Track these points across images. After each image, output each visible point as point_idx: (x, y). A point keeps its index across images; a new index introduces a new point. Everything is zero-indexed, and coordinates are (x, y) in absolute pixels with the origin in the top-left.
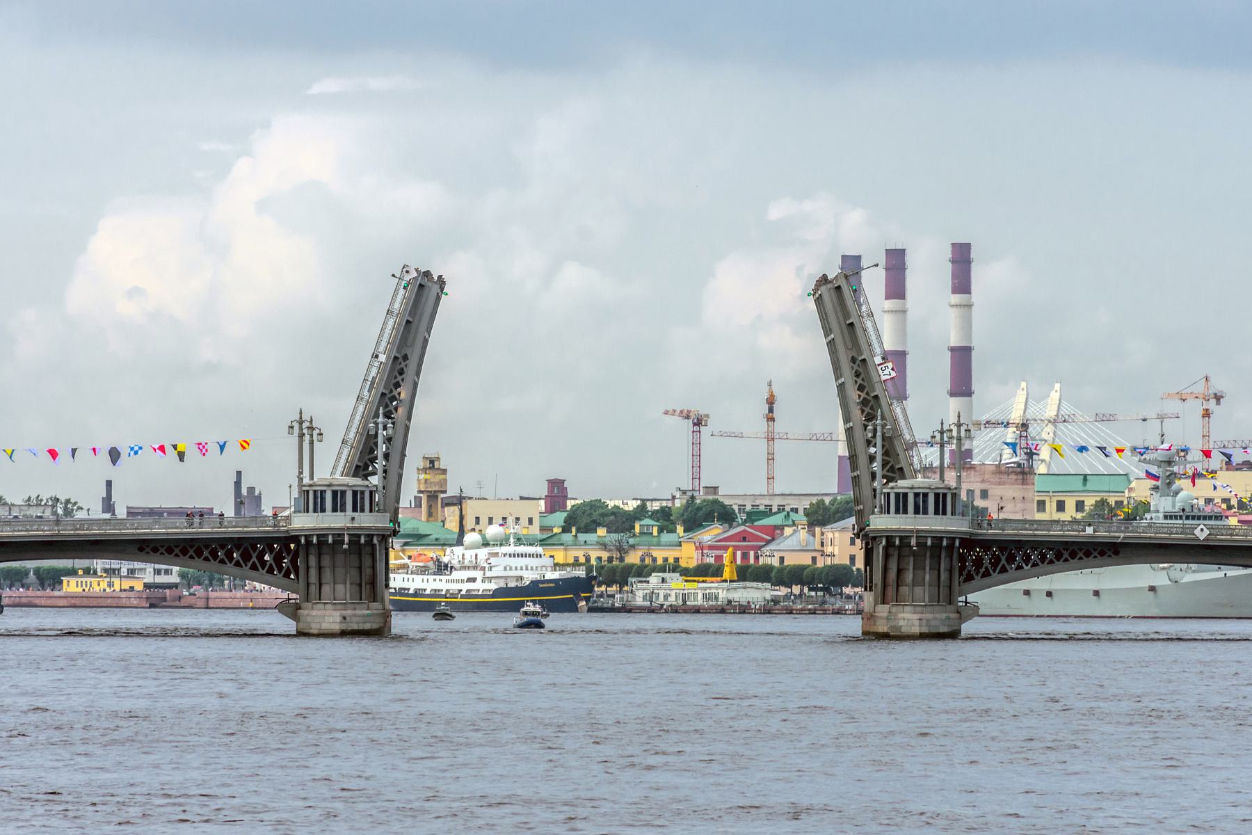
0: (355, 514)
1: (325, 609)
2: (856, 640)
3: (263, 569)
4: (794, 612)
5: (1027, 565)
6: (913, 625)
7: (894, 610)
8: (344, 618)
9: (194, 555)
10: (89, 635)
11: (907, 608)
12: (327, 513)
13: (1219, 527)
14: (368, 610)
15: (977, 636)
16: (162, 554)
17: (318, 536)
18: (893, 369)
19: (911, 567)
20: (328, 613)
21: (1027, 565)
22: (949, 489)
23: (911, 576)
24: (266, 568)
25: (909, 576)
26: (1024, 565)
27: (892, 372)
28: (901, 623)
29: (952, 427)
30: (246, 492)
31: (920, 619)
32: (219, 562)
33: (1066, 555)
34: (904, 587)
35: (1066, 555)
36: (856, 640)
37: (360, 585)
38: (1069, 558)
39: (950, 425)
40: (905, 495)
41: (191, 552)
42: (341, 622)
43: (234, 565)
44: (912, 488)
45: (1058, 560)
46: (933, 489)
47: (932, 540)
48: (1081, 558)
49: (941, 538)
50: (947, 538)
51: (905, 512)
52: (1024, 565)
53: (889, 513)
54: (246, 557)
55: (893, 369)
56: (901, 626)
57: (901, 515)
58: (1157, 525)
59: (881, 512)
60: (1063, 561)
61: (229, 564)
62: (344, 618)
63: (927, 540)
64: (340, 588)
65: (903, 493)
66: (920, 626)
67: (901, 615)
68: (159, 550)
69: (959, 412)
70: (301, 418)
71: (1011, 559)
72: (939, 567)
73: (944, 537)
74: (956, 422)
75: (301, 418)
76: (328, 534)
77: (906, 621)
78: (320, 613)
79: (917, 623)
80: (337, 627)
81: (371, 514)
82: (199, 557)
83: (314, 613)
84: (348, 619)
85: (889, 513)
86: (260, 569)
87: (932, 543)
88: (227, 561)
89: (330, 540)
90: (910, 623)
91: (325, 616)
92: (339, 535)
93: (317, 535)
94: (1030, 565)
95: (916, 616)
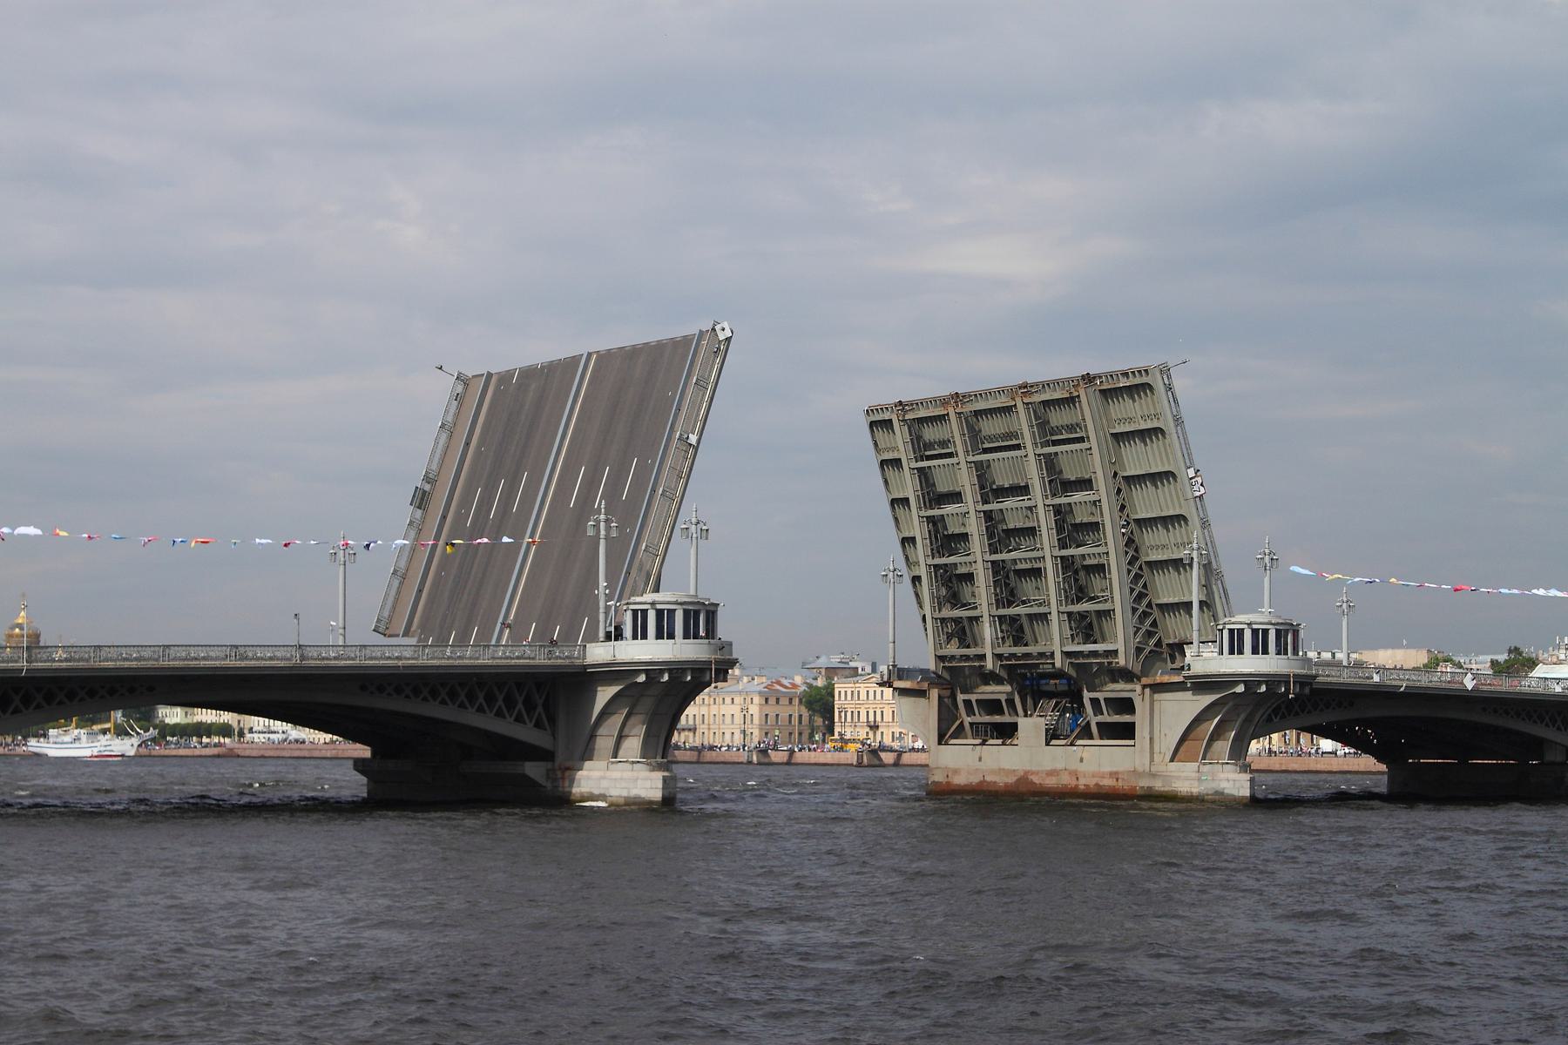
3: (491, 712)
6: (1242, 787)
9: (446, 698)
16: (389, 694)
18: (1202, 485)
27: (1201, 487)
30: (1412, 652)
32: (495, 715)
38: (430, 698)
40: (1241, 631)
41: (462, 697)
45: (1315, 710)
49: (684, 670)
51: (1265, 652)
54: (490, 699)
55: (1202, 485)
60: (35, 708)
61: (470, 710)
67: (1222, 776)
77: (1231, 782)
82: (435, 700)
86: (507, 716)
88: (468, 706)
90: (1237, 785)
91: (637, 779)
94: (1278, 717)
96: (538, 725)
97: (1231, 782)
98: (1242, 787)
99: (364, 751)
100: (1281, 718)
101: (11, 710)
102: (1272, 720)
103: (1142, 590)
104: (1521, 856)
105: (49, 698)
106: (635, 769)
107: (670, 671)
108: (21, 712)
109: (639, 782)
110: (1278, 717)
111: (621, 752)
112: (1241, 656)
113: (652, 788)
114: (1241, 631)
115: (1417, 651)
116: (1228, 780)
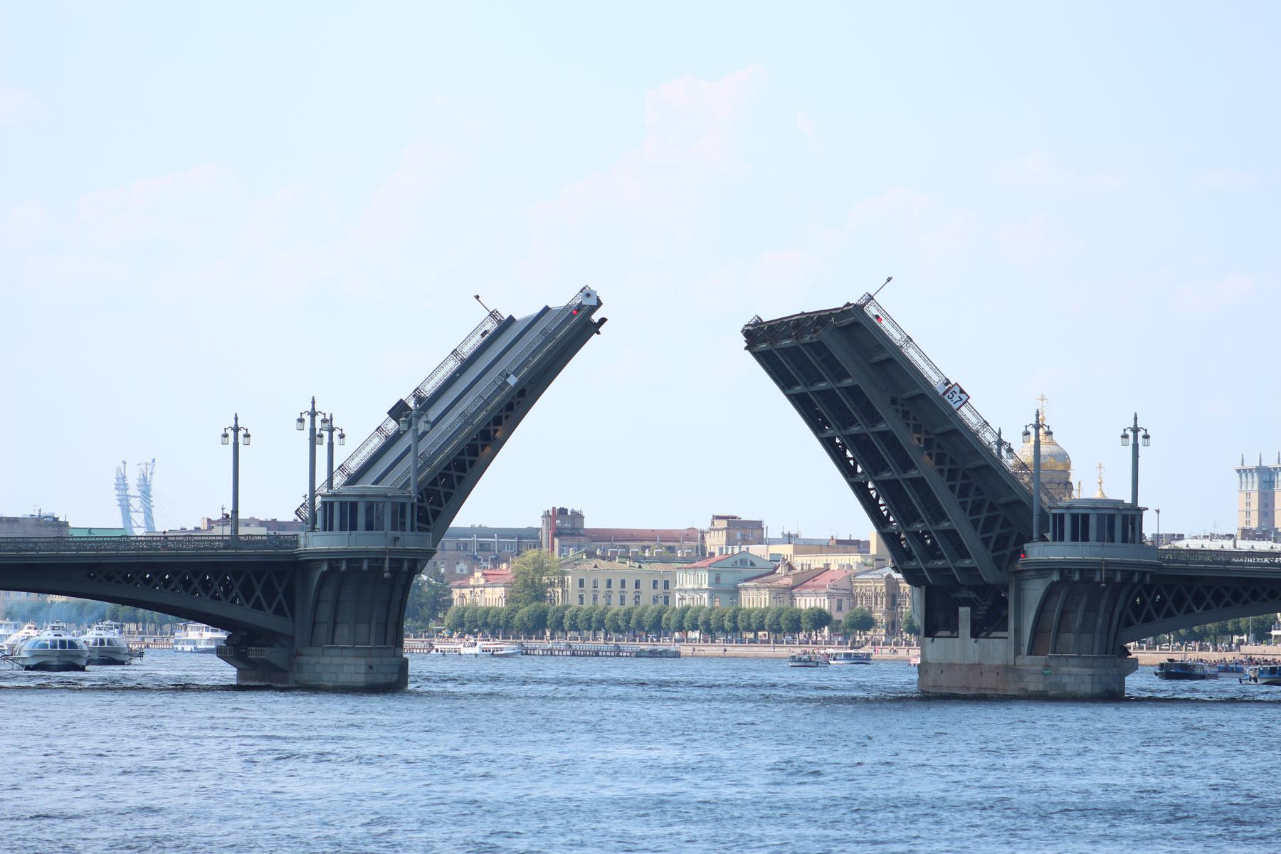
0: (398, 533)
1: (342, 656)
2: (900, 700)
4: (600, 653)
5: (1198, 608)
6: (1084, 682)
7: (1052, 663)
8: (371, 667)
10: (71, 689)
11: (1071, 661)
12: (359, 532)
13: (17, 540)
14: (394, 656)
15: (1161, 695)
16: (118, 582)
17: (1081, 571)
19: (1082, 608)
20: (348, 661)
21: (1198, 608)
22: (1118, 509)
23: (1079, 621)
24: (252, 603)
25: (1078, 620)
26: (1195, 608)
28: (1066, 679)
29: (228, 431)
31: (1092, 675)
33: (1228, 597)
34: (1067, 634)
35: (1228, 597)
36: (900, 700)
37: (386, 625)
39: (1125, 430)
40: (1062, 516)
42: (366, 673)
43: (972, 521)
44: (1068, 508)
46: (1122, 510)
47: (1122, 575)
48: (1264, 600)
49: (1133, 573)
50: (408, 560)
52: (1195, 608)
53: (1112, 540)
56: (1065, 684)
57: (1080, 543)
58: (195, 538)
59: (1054, 540)
62: (371, 667)
63: (362, 563)
64: (363, 628)
65: (1109, 515)
66: (1092, 683)
67: (1064, 670)
68: (908, 419)
69: (1038, 410)
70: (313, 409)
71: (1179, 600)
72: (1114, 609)
73: (1135, 571)
74: (1132, 426)
75: (313, 409)
76: (362, 559)
77: (1073, 677)
78: (335, 660)
79: (1088, 679)
80: (360, 680)
81: (1123, 544)
83: (327, 660)
84: (375, 668)
85: (1112, 540)
87: (369, 567)
89: (365, 566)
91: (343, 665)
92: (377, 560)
93: (348, 559)
94: (1201, 609)
95: (1089, 671)
96: (279, 611)
97: (1073, 677)
98: (1084, 682)
99: (222, 635)
100: (1205, 609)
101: (1222, 604)
102: (1192, 611)
103: (964, 482)
104: (1180, 789)
105: (1237, 596)
106: (344, 654)
107: (1061, 571)
108: (1231, 605)
109: (345, 667)
110: (1201, 609)
111: (336, 639)
112: (1112, 544)
113: (356, 673)
114: (1062, 516)
115: (233, 519)
116: (1070, 675)
